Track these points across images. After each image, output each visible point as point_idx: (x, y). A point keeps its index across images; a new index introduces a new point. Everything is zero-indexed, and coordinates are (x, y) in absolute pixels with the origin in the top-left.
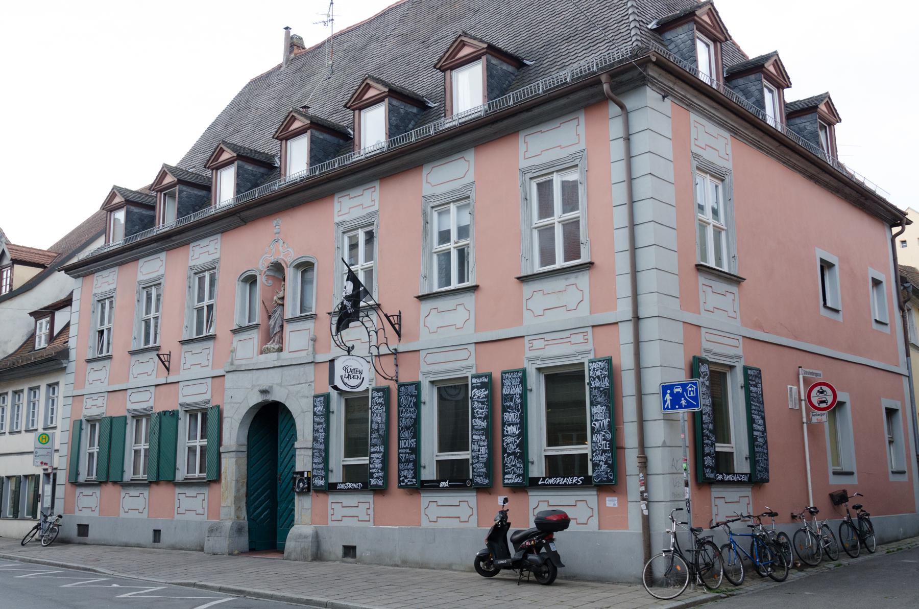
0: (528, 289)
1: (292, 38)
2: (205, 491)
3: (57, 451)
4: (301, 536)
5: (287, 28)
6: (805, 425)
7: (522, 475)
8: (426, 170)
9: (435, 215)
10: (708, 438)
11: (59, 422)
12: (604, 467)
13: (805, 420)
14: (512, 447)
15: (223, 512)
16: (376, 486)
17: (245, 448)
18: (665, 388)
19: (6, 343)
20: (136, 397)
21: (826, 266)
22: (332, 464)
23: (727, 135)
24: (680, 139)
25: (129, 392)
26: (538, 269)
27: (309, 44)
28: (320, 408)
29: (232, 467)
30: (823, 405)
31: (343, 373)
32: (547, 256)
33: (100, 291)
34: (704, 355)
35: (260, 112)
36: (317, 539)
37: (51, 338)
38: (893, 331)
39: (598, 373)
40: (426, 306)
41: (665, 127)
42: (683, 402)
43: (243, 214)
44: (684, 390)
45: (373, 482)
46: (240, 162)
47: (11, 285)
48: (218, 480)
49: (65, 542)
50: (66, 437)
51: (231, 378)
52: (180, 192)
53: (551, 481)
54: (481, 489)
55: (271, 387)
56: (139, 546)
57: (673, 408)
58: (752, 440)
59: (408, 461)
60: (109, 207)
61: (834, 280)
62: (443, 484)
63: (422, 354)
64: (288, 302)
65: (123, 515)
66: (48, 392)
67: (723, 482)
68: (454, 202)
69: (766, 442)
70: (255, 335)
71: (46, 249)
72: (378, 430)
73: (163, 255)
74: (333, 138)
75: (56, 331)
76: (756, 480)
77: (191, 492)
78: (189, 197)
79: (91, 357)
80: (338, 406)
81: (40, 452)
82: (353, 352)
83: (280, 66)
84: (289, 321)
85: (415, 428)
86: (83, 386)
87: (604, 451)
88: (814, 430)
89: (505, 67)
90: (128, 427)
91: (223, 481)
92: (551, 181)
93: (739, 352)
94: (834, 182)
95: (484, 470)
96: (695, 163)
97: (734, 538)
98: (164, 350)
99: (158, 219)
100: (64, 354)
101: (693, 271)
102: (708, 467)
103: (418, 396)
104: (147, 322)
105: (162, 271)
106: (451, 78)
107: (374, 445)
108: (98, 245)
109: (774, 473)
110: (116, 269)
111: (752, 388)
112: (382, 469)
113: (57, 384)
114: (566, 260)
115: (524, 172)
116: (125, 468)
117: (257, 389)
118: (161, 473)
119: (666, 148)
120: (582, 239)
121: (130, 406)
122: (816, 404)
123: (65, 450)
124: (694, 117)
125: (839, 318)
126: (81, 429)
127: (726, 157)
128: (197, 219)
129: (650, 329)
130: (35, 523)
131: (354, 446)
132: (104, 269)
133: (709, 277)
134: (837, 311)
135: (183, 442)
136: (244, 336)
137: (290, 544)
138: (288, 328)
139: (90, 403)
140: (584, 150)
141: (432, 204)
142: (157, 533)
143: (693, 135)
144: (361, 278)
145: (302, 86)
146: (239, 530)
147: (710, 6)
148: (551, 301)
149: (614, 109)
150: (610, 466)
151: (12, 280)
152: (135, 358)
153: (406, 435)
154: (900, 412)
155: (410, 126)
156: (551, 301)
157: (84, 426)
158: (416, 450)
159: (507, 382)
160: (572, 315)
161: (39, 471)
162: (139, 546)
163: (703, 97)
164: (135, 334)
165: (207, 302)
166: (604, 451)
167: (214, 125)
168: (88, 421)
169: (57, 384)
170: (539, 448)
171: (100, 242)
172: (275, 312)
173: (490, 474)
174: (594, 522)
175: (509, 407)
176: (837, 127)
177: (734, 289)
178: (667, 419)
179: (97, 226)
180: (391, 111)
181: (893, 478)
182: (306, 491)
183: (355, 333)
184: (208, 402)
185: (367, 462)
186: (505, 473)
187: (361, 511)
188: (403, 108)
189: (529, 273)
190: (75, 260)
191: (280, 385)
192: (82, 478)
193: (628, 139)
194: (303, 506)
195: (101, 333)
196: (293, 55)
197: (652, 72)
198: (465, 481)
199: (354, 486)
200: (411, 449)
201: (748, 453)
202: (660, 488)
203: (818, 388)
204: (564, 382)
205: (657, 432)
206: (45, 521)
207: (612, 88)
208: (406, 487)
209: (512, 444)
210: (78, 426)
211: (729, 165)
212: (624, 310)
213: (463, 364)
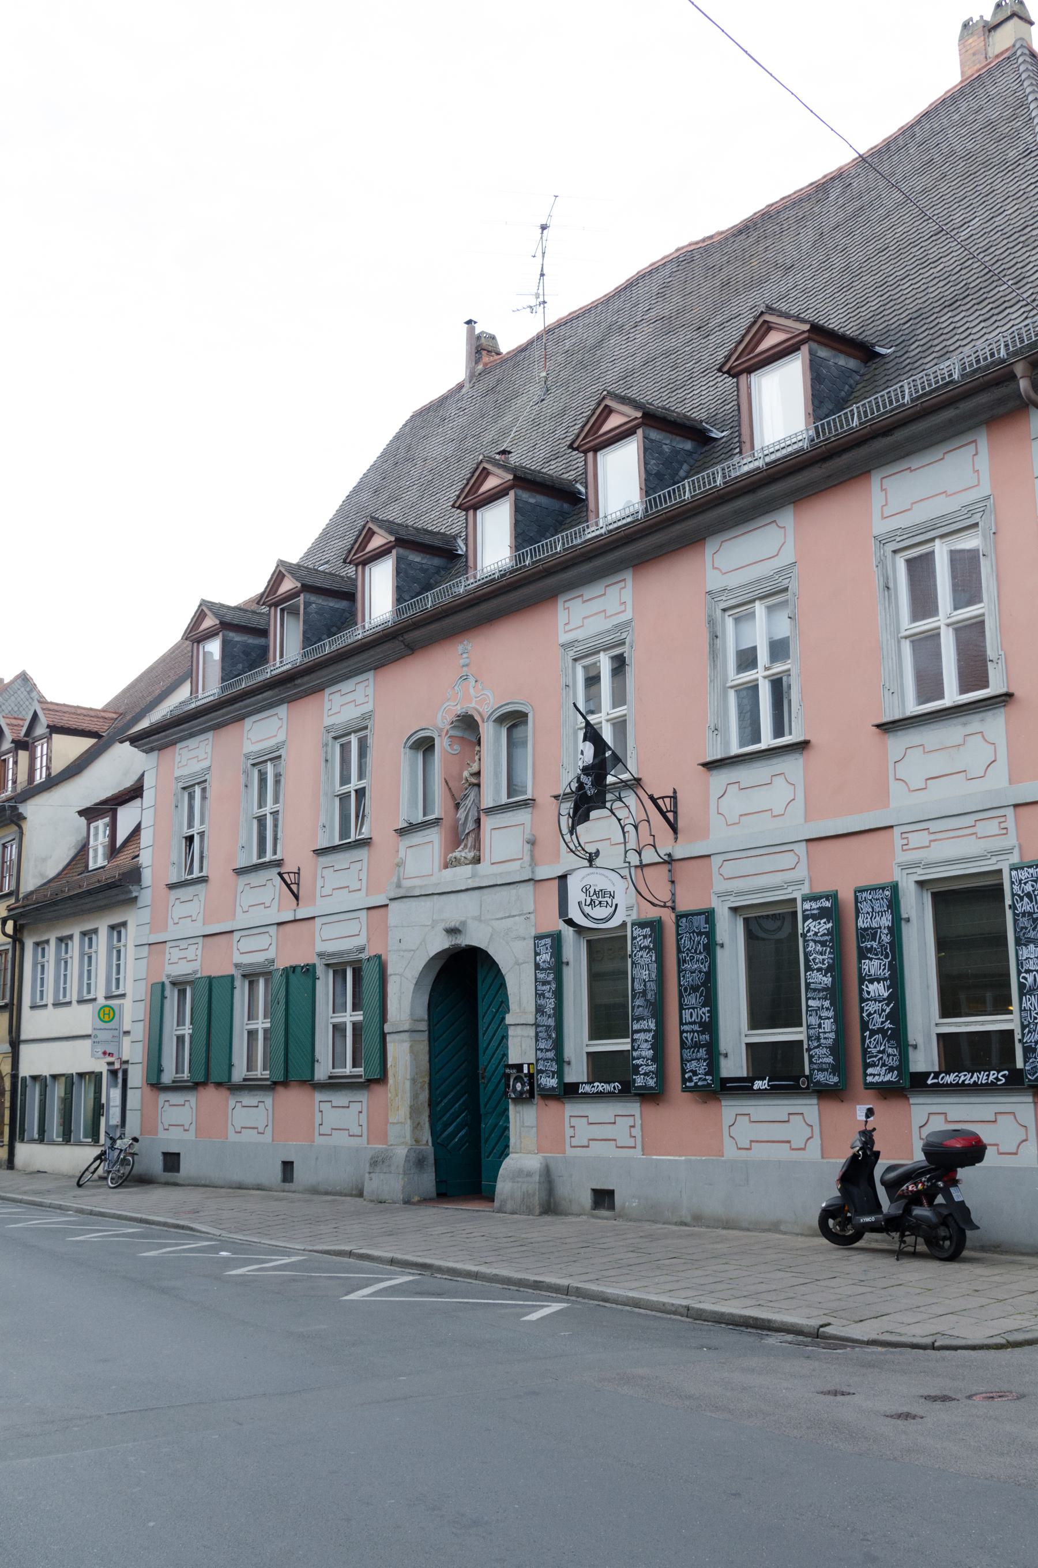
0: (897, 743)
1: (479, 337)
2: (363, 1096)
3: (127, 1033)
5: (469, 322)
8: (711, 547)
9: (730, 623)
15: (393, 1132)
16: (645, 1087)
17: (424, 1026)
19: (44, 860)
20: (247, 944)
25: (169, 944)
26: (912, 708)
27: (506, 346)
28: (545, 957)
29: (404, 1058)
31: (582, 897)
32: (929, 684)
33: (185, 771)
36: (548, 1177)
37: (113, 851)
40: (720, 779)
45: (639, 1081)
46: (401, 550)
47: (48, 768)
49: (144, 1181)
52: (307, 604)
55: (464, 923)
56: (259, 1188)
59: (697, 1046)
60: (195, 636)
62: (758, 1085)
63: (716, 861)
65: (232, 1137)
70: (434, 840)
72: (644, 993)
73: (282, 710)
74: (551, 501)
75: (120, 840)
77: (340, 1098)
78: (320, 612)
79: (174, 880)
81: (103, 1036)
82: (598, 862)
83: (460, 386)
85: (706, 989)
86: (165, 928)
89: (842, 361)
91: (391, 1080)
95: (830, 1060)
99: (276, 649)
100: (134, 875)
103: (710, 934)
106: (749, 387)
107: (639, 1019)
110: (210, 735)
112: (654, 1059)
113: (124, 924)
114: (964, 689)
115: (882, 541)
116: (235, 1060)
118: (290, 1068)
120: (990, 653)
121: (238, 959)
123: (139, 1032)
126: (163, 997)
128: (334, 648)
130: (96, 1151)
131: (606, 1019)
132: (192, 735)
135: (325, 1017)
136: (417, 838)
137: (504, 1186)
139: (176, 954)
140: (988, 498)
142: (288, 1166)
144: (607, 735)
146: (420, 1162)
148: (937, 764)
151: (49, 759)
152: (324, 860)
153: (691, 1000)
155: (682, 473)
156: (937, 764)
157: (167, 993)
158: (710, 1027)
159: (865, 907)
161: (101, 1066)
162: (259, 1188)
164: (242, 841)
165: (354, 784)
168: (174, 984)
170: (926, 1020)
171: (183, 693)
172: (466, 797)
173: (840, 1065)
175: (870, 950)
183: (599, 829)
184: (362, 950)
186: (867, 1066)
187: (621, 1131)
188: (670, 443)
189: (897, 717)
190: (157, 715)
191: (479, 919)
192: (167, 1078)
194: (523, 1122)
195: (190, 839)
196: (480, 367)
199: (608, 1088)
206: (112, 1148)
209: (877, 1014)
213: (787, 878)
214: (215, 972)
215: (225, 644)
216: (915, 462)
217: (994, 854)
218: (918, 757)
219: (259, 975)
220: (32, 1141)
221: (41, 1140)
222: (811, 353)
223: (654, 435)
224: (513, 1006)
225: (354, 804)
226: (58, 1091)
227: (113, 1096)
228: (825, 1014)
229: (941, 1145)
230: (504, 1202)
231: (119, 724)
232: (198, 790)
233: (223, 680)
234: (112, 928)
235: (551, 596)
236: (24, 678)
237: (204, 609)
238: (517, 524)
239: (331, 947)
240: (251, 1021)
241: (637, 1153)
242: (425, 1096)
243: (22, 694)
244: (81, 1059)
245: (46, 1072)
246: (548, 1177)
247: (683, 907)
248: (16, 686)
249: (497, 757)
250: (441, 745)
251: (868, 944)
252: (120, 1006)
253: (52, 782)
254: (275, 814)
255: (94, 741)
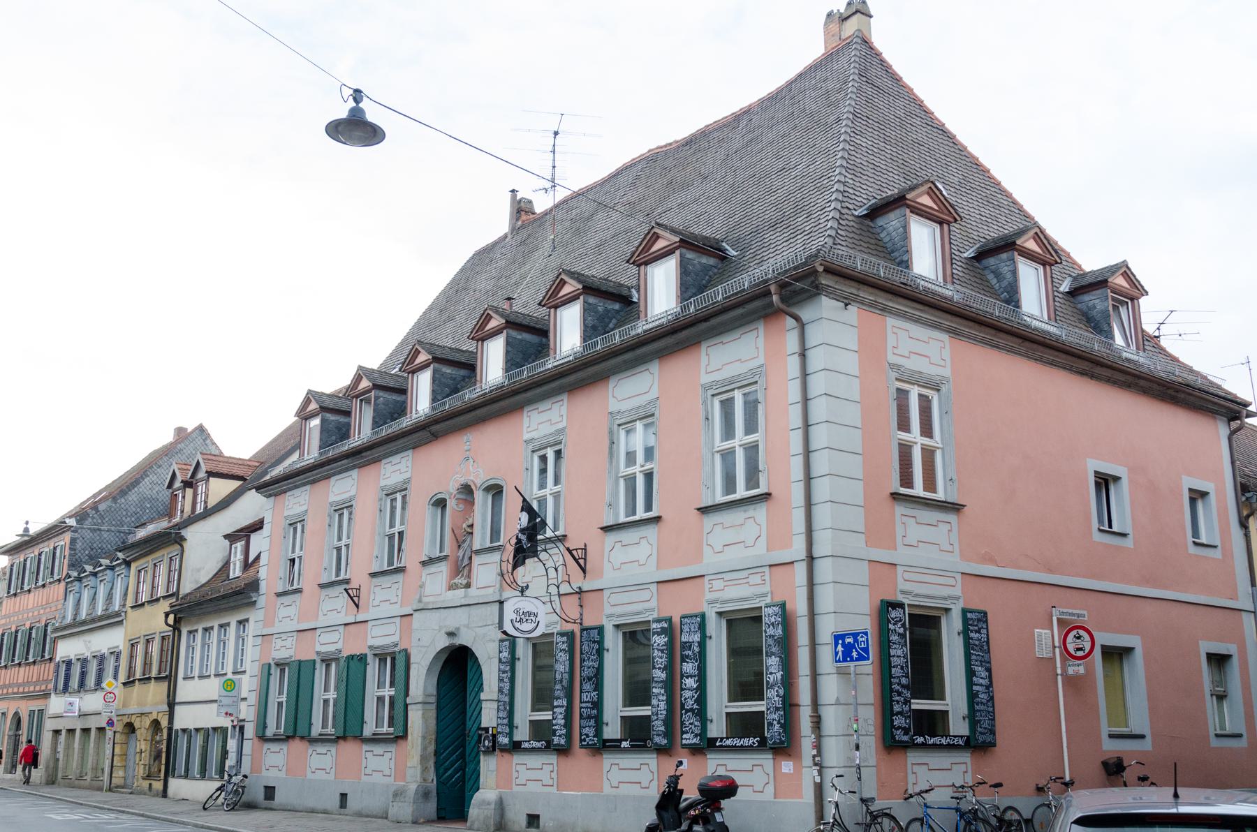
0: (710, 520)
1: (520, 201)
2: (392, 747)
3: (244, 699)
4: (485, 803)
5: (513, 191)
6: (1059, 678)
7: (700, 735)
8: (612, 382)
9: (622, 434)
10: (899, 694)
11: (247, 666)
12: (777, 726)
13: (1059, 671)
14: (690, 702)
15: (409, 772)
16: (558, 745)
17: (433, 699)
18: (838, 638)
19: (199, 570)
20: (325, 638)
21: (1104, 482)
22: (517, 720)
23: (945, 337)
24: (871, 351)
25: (318, 631)
26: (720, 498)
27: (539, 208)
28: (505, 654)
29: (419, 721)
30: (1080, 654)
31: (514, 616)
32: (730, 485)
33: (292, 513)
34: (900, 598)
35: (478, 294)
36: (501, 805)
37: (247, 565)
38: (1228, 553)
39: (773, 620)
40: (611, 538)
41: (850, 339)
42: (854, 654)
43: (435, 428)
44: (856, 640)
45: (556, 740)
46: (437, 365)
47: (206, 503)
48: (404, 736)
49: (251, 806)
50: (254, 684)
51: (417, 617)
52: (377, 398)
53: (728, 742)
54: (662, 751)
55: (458, 629)
56: (325, 812)
57: (845, 660)
58: (972, 696)
59: (589, 717)
60: (304, 415)
61: (1121, 497)
62: (625, 744)
63: (606, 593)
64: (477, 530)
65: (309, 776)
66: (238, 629)
67: (924, 746)
68: (739, 388)
69: (992, 698)
70: (443, 569)
71: (247, 457)
72: (561, 681)
73: (355, 473)
74: (611, 301)
75: (251, 559)
76: (979, 743)
77: (378, 749)
78: (386, 403)
79: (281, 590)
80: (525, 654)
81: (226, 701)
82: (527, 593)
83: (506, 236)
84: (477, 552)
85: (597, 679)
86: (273, 624)
87: (777, 709)
88: (1071, 682)
89: (705, 260)
90: (317, 672)
91: (409, 737)
92: (733, 398)
93: (957, 591)
94: (1122, 377)
95: (663, 728)
96: (894, 375)
97: (929, 811)
98: (354, 584)
99: (356, 428)
100: (254, 585)
101: (889, 501)
102: (899, 728)
103: (601, 642)
104: (339, 549)
105: (353, 493)
106: (646, 274)
107: (558, 698)
108: (293, 461)
109: (1004, 736)
110: (308, 487)
111: (972, 635)
112: (565, 726)
113: (247, 620)
114: (748, 489)
115: (706, 388)
116: (313, 721)
117: (443, 632)
118: (349, 730)
119: (851, 363)
120: (761, 468)
121: (319, 648)
122: (1072, 652)
123: (253, 699)
124: (891, 321)
125: (1128, 543)
126: (269, 674)
127: (942, 363)
128: (390, 431)
129: (824, 570)
130: (218, 784)
131: (541, 698)
132: (296, 487)
133: (908, 505)
134: (1124, 535)
135: (372, 691)
136: (433, 568)
137: (474, 812)
138: (477, 560)
139: (279, 643)
140: (762, 366)
141: (619, 422)
142: (344, 796)
143: (891, 341)
144: (535, 506)
145: (523, 264)
146: (426, 795)
147: (930, 185)
148: (730, 536)
149: (790, 322)
150: (783, 726)
151: (207, 496)
152: (325, 592)
153: (588, 686)
154: (1235, 661)
155: (611, 325)
156: (730, 536)
157: (272, 671)
158: (598, 705)
159: (686, 628)
160: (750, 552)
161: (226, 722)
162: (325, 812)
163: (901, 300)
164: (325, 564)
165: (343, 543)
166: (777, 709)
167: (430, 309)
168: (277, 665)
169: (247, 620)
170: (719, 703)
171: (295, 457)
172: (464, 541)
173: (669, 733)
174: (770, 789)
175: (687, 656)
176: (1143, 301)
177: (952, 517)
178: (842, 673)
179: (290, 441)
180: (587, 310)
181: (1215, 742)
182: (492, 750)
183: (531, 571)
184: (396, 645)
185: (649, 713)
186: (683, 733)
187: (545, 775)
188: (601, 305)
189: (710, 504)
190: (277, 471)
191: (467, 626)
192: (270, 732)
193: (803, 355)
194: (489, 766)
195: (293, 561)
196: (520, 223)
197: (825, 280)
198: (645, 741)
199: (538, 745)
200: (592, 703)
201: (966, 712)
202: (834, 752)
203: (1074, 633)
204: (743, 625)
205: (831, 687)
206: (229, 782)
207: (783, 300)
208: (588, 746)
209: (689, 698)
210: (267, 670)
211: (947, 372)
212: (798, 549)
213: (644, 607)
214: (304, 656)
215: (323, 421)
216: (725, 338)
217: (758, 596)
218: (721, 530)
219: (332, 660)
220: (180, 777)
221: (186, 777)
222: (681, 256)
223: (592, 300)
224: (486, 687)
225: (396, 542)
226: (199, 740)
227: (232, 745)
228: (661, 698)
229: (707, 785)
230: (473, 822)
231: (260, 470)
232: (299, 526)
233: (321, 448)
234: (240, 622)
235: (518, 408)
236: (201, 429)
237: (311, 396)
238: (507, 353)
239: (324, 649)
240: (325, 692)
241: (554, 790)
242: (432, 748)
243: (199, 441)
244: (209, 717)
245: (191, 726)
246: (501, 805)
247: (587, 623)
248: (194, 435)
249: (484, 515)
250: (451, 504)
251: (686, 653)
252: (240, 680)
253: (208, 513)
254: (347, 546)
255: (240, 483)
